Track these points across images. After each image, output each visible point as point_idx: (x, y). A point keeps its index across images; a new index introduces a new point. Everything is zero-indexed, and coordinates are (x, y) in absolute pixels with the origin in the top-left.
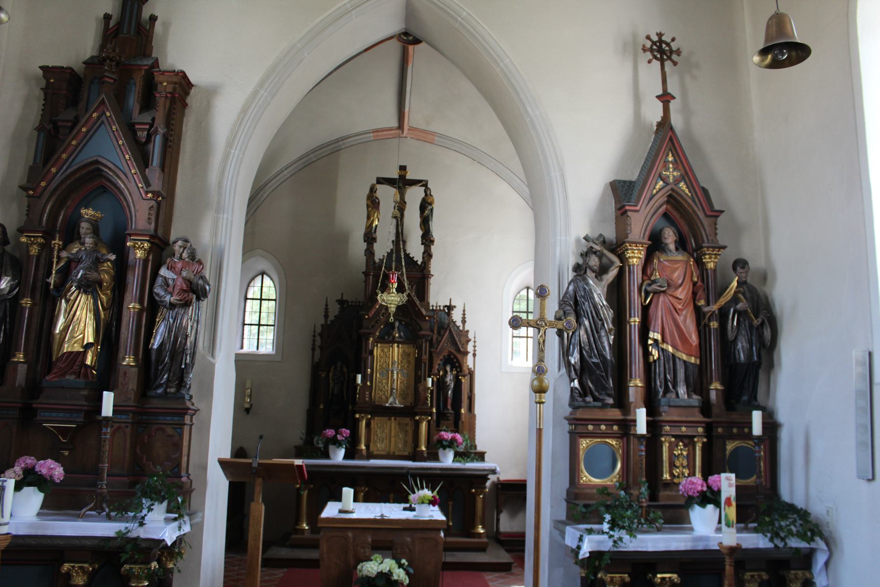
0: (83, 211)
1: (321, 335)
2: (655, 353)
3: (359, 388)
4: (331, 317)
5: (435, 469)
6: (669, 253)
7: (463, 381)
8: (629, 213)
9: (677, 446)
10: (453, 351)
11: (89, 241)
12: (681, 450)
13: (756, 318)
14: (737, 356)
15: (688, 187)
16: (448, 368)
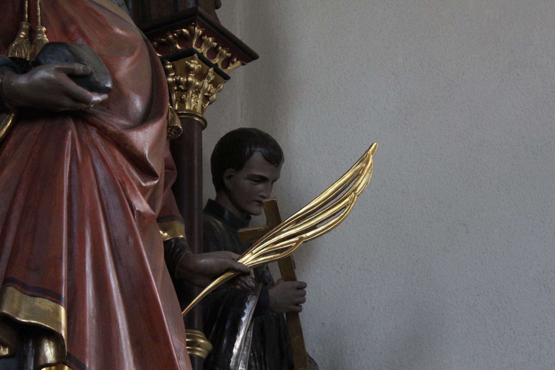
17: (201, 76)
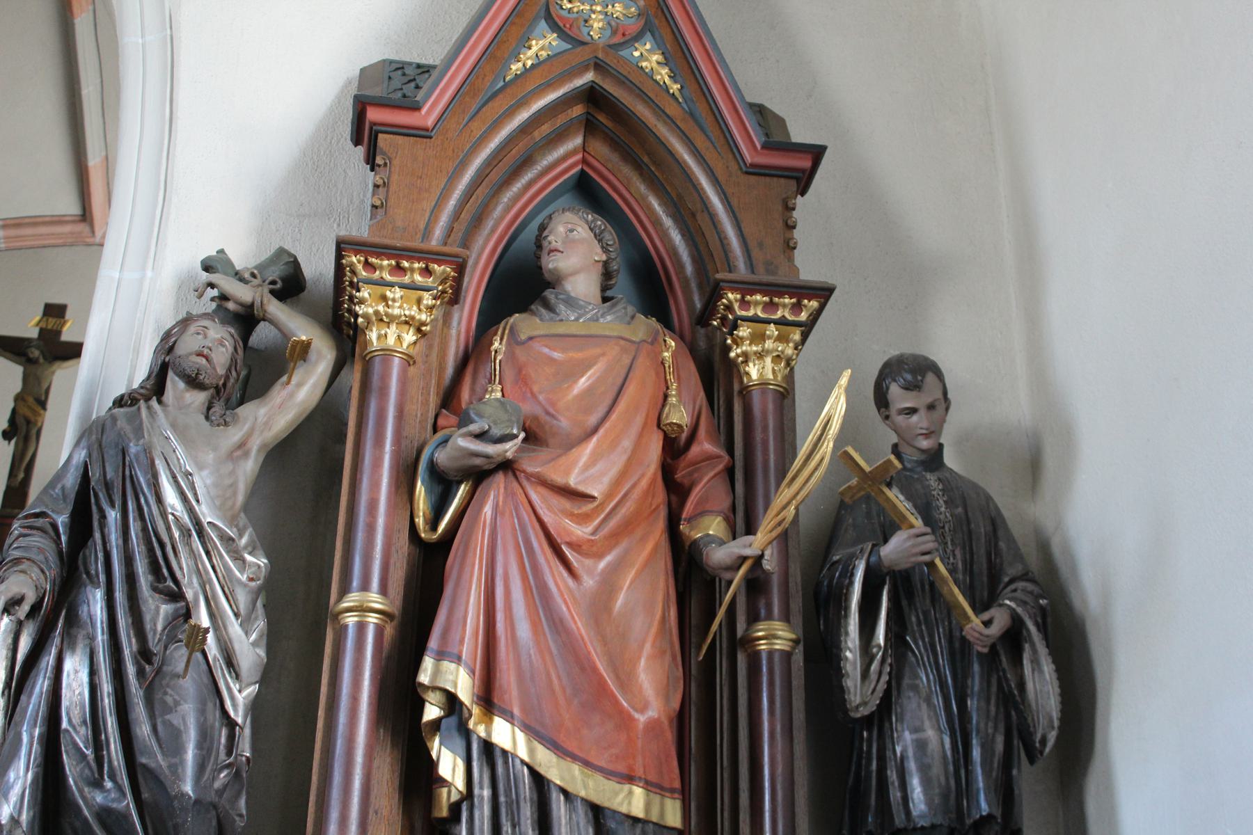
6: (562, 308)
14: (895, 794)
17: (759, 338)
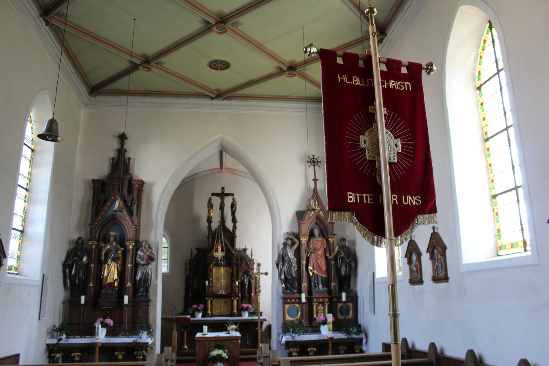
0: (111, 233)
1: (189, 264)
2: (311, 274)
3: (207, 287)
4: (194, 255)
5: (240, 320)
7: (252, 281)
8: (301, 225)
9: (319, 306)
10: (247, 268)
11: (114, 244)
12: (321, 307)
13: (348, 259)
15: (323, 213)
16: (245, 276)
